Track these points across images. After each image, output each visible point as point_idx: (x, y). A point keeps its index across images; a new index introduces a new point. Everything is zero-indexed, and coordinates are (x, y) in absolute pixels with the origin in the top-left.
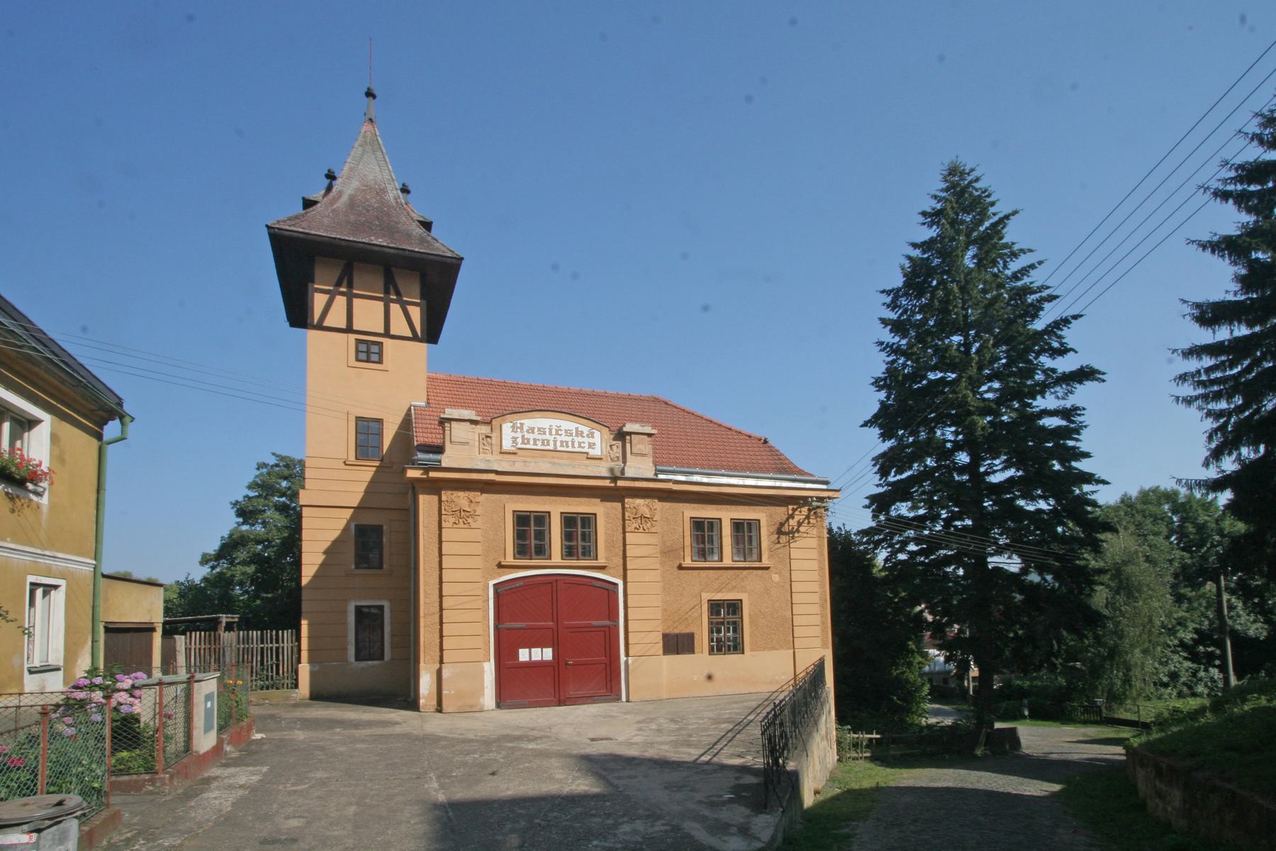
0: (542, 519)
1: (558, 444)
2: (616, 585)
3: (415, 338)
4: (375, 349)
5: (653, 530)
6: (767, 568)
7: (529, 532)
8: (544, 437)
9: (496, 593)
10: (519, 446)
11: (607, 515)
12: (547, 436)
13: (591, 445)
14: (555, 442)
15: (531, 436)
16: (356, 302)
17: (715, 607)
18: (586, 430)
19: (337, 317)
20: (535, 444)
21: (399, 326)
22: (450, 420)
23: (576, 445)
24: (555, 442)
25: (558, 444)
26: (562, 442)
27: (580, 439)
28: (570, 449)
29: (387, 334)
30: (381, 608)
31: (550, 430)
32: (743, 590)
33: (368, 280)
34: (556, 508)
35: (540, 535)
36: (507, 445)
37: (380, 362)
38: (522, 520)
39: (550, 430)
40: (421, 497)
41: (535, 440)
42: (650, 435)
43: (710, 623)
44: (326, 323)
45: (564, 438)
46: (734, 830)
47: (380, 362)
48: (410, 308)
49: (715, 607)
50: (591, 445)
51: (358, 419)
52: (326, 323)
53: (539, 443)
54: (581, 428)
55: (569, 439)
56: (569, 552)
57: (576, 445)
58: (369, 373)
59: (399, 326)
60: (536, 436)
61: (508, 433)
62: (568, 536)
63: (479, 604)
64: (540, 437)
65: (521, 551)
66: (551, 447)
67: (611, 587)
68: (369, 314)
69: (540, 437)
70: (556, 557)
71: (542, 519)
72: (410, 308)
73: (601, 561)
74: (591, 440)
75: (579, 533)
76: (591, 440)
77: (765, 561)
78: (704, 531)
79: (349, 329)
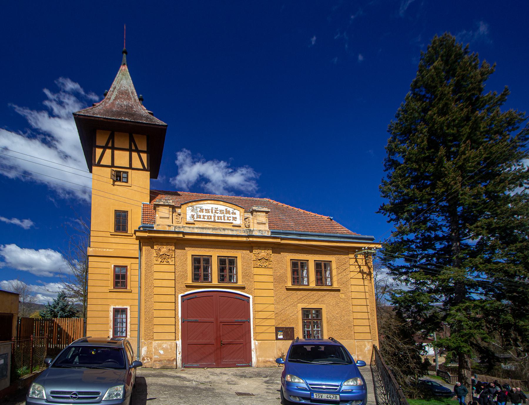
0: (207, 260)
1: (216, 218)
2: (249, 298)
3: (144, 169)
4: (125, 175)
5: (270, 266)
6: (339, 290)
7: (200, 267)
8: (208, 214)
9: (183, 301)
10: (195, 219)
11: (243, 258)
12: (210, 214)
13: (235, 219)
14: (214, 217)
15: (201, 214)
16: (116, 152)
17: (306, 312)
18: (231, 210)
19: (107, 160)
20: (204, 218)
21: (137, 163)
22: (159, 205)
23: (226, 218)
24: (214, 217)
25: (216, 218)
26: (218, 217)
27: (228, 215)
28: (223, 221)
29: (131, 168)
30: (127, 309)
31: (212, 210)
32: (323, 302)
33: (122, 141)
34: (215, 254)
35: (206, 269)
36: (189, 219)
37: (127, 182)
38: (196, 260)
39: (212, 210)
40: (143, 247)
41: (204, 216)
42: (267, 212)
43: (303, 322)
44: (101, 163)
45: (219, 215)
46: (58, 150)
47: (127, 182)
48: (141, 154)
49: (306, 312)
50: (235, 219)
51: (116, 211)
52: (101, 163)
53: (206, 217)
54: (229, 209)
55: (222, 215)
56: (222, 279)
57: (226, 218)
58: (120, 189)
59: (137, 163)
60: (204, 214)
61: (189, 212)
62: (222, 270)
63: (259, 329)
64: (207, 214)
65: (196, 278)
66: (212, 220)
67: (247, 299)
68: (122, 158)
69: (207, 214)
70: (215, 281)
71: (207, 260)
72: (141, 154)
73: (240, 283)
74: (234, 216)
75: (227, 267)
76: (234, 216)
77: (335, 286)
78: (297, 268)
79: (113, 166)
